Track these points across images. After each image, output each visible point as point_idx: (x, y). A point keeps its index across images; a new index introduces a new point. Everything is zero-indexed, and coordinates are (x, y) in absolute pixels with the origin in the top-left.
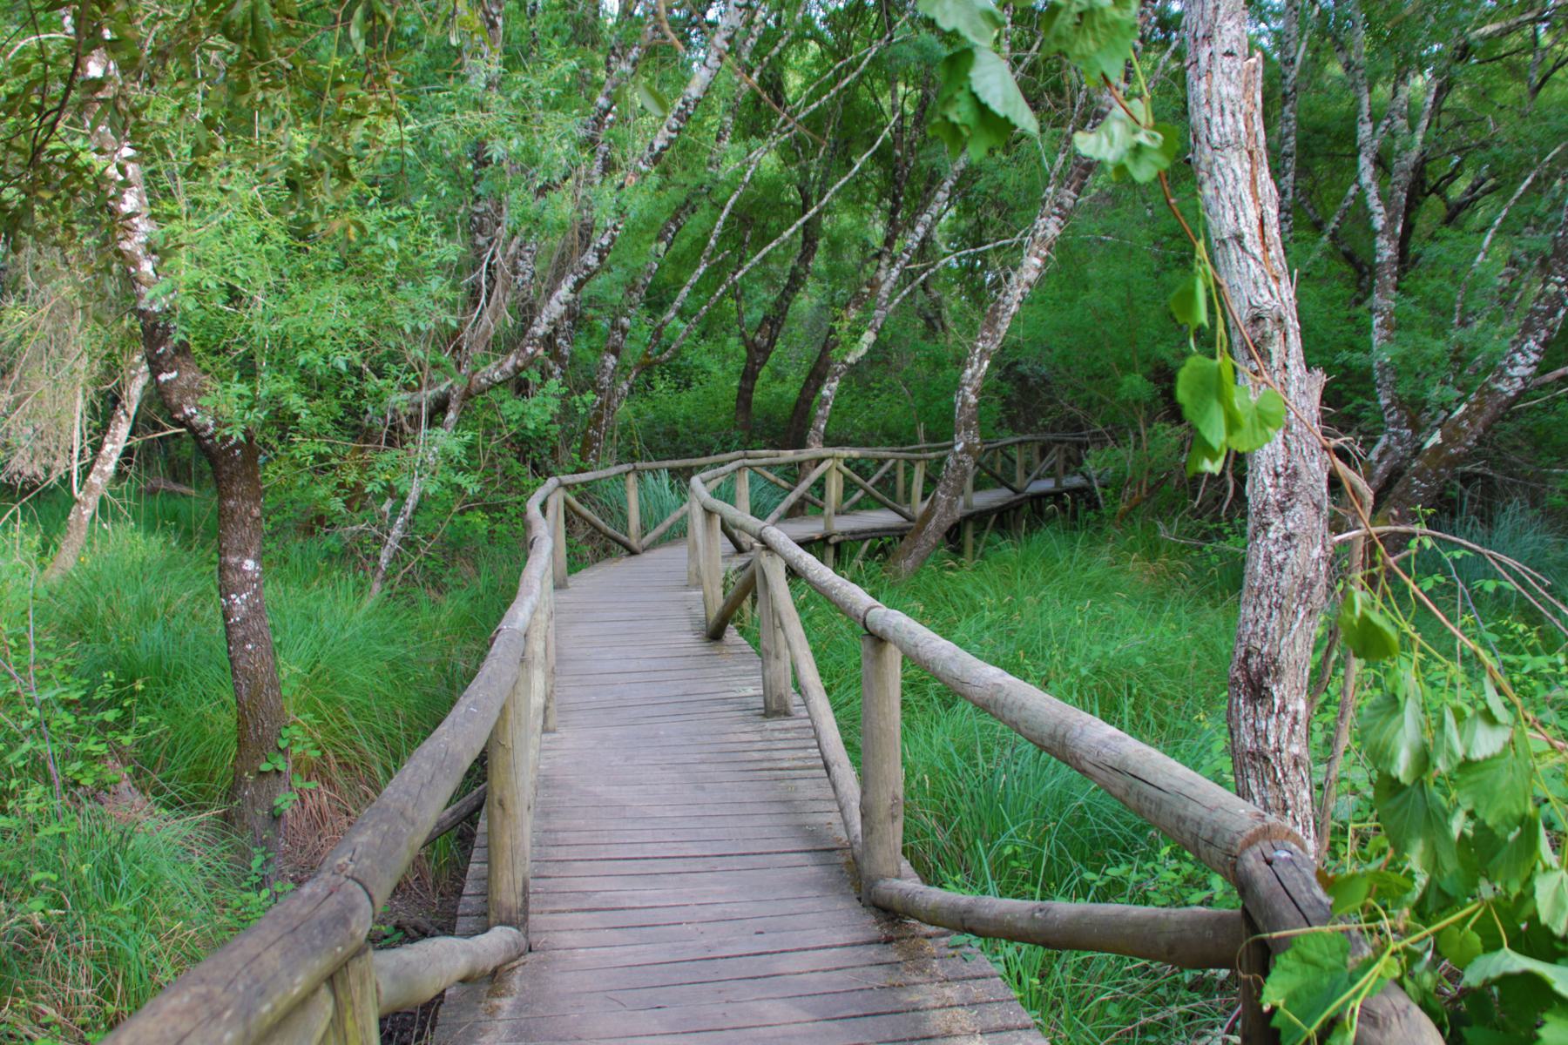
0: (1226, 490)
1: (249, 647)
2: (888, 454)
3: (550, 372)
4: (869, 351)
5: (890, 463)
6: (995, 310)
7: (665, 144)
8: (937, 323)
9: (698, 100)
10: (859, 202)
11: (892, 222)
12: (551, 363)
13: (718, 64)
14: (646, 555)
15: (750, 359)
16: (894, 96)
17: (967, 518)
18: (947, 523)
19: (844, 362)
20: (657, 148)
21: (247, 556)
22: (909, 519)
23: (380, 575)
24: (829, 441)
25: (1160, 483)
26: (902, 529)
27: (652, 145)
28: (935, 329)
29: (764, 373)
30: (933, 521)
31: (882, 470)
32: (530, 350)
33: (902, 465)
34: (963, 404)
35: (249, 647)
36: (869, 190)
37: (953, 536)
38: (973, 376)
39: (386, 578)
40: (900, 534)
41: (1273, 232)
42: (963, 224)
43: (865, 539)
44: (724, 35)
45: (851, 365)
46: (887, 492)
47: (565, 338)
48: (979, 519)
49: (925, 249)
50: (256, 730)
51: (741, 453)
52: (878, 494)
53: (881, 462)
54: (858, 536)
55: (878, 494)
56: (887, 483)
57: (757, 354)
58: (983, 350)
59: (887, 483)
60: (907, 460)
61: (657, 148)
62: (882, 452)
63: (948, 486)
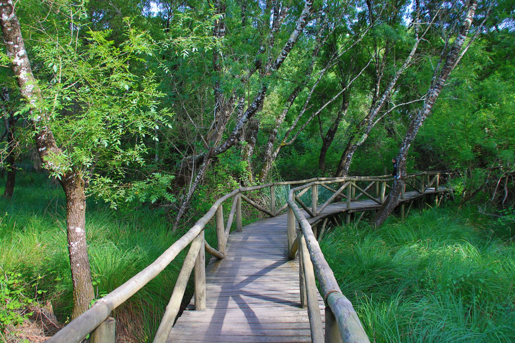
0: (504, 193)
1: (78, 265)
2: (372, 179)
3: (248, 149)
4: (365, 141)
5: (373, 182)
6: (413, 125)
7: (281, 60)
8: (392, 132)
9: (293, 43)
10: (364, 89)
11: (375, 96)
12: (249, 146)
13: (301, 29)
14: (277, 217)
15: (324, 144)
16: (376, 51)
17: (401, 203)
18: (394, 206)
19: (356, 145)
20: (278, 62)
21: (78, 226)
22: (380, 204)
23: (176, 223)
24: (350, 174)
25: (477, 191)
26: (377, 207)
27: (276, 61)
28: (391, 134)
29: (330, 148)
30: (388, 205)
31: (371, 184)
32: (232, 140)
33: (378, 183)
34: (400, 161)
35: (78, 265)
36: (367, 85)
37: (397, 211)
38: (404, 150)
39: (179, 224)
40: (377, 210)
41: (317, 222)
42: (401, 97)
43: (363, 211)
44: (303, 17)
45: (358, 146)
46: (373, 193)
47: (254, 136)
48: (407, 204)
49: (387, 105)
50: (80, 301)
51: (316, 179)
52: (367, 194)
53: (371, 182)
54: (360, 210)
55: (367, 194)
56: (372, 190)
57: (327, 142)
58: (408, 140)
59: (372, 190)
60: (380, 181)
61: (278, 62)
62: (368, 178)
63: (394, 192)
